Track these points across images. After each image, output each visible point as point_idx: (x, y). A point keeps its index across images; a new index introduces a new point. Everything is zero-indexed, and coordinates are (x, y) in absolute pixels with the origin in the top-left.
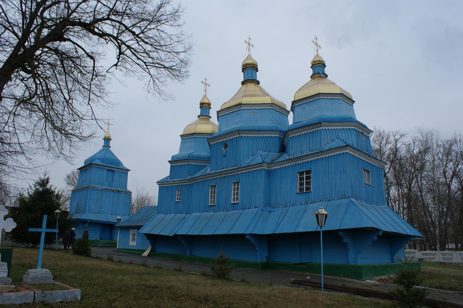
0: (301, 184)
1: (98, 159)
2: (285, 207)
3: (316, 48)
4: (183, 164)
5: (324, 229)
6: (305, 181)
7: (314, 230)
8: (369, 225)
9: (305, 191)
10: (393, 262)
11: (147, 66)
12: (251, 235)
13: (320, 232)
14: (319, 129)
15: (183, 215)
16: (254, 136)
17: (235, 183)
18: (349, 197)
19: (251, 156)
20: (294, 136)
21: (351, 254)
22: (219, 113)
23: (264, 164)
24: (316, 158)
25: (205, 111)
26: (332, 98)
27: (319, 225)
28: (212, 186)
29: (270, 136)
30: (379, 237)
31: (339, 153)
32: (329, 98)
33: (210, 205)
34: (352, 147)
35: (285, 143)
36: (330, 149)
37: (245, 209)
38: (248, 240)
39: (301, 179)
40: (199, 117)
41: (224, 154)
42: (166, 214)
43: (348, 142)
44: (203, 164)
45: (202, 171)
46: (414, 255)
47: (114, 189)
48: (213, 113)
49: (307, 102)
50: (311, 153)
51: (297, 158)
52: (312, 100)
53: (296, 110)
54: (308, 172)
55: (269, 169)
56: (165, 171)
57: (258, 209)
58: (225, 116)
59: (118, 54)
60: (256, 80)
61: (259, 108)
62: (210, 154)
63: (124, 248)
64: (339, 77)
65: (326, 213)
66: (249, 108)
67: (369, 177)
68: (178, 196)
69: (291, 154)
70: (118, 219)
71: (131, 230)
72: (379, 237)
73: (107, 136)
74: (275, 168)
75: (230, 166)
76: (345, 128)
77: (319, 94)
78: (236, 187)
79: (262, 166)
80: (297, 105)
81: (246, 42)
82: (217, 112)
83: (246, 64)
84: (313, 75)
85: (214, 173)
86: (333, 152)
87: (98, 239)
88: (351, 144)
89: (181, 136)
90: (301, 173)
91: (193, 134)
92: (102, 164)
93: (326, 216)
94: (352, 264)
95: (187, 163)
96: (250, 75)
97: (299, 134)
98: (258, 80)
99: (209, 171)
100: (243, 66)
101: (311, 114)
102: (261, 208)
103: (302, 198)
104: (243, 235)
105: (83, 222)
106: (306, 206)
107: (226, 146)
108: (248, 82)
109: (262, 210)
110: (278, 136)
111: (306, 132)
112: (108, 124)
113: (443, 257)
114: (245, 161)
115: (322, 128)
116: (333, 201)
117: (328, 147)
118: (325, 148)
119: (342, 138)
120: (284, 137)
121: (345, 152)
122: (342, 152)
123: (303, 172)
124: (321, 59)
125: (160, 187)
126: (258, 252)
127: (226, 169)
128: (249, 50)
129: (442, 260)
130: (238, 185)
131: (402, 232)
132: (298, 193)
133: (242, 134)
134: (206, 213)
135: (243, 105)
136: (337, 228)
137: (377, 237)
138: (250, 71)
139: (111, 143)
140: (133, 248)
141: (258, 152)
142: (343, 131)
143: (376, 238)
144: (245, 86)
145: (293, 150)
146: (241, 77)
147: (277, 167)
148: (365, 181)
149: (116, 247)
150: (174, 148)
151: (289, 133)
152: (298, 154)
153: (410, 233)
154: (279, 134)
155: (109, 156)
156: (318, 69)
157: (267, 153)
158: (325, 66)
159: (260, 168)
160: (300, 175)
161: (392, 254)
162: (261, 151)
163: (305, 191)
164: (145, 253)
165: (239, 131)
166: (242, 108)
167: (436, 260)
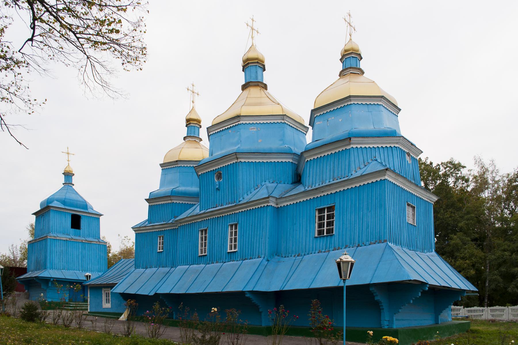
0: (321, 225)
1: (57, 201)
2: (298, 256)
3: (349, 31)
4: (164, 202)
5: (349, 283)
6: (326, 221)
7: (336, 285)
8: (414, 277)
9: (325, 234)
10: (437, 323)
11: (78, 38)
12: (252, 292)
13: (342, 287)
14: (348, 148)
15: (167, 269)
16: (257, 161)
17: (232, 226)
18: (385, 241)
19: (253, 190)
20: (312, 158)
21: (386, 316)
22: (209, 130)
23: (271, 199)
24: (342, 189)
25: (193, 131)
26: (368, 103)
27: (341, 277)
28: (202, 231)
29: (280, 161)
30: (424, 293)
31: (374, 181)
32: (364, 103)
33: (200, 255)
34: (394, 172)
35: (300, 171)
36: (362, 176)
37: (246, 259)
38: (248, 298)
39: (321, 218)
40: (185, 138)
41: (217, 187)
42: (146, 268)
43: (388, 166)
44: (191, 203)
45: (190, 211)
46: (458, 312)
47: (83, 239)
48: (203, 133)
49: (332, 109)
50: (335, 181)
51: (316, 189)
52: (339, 107)
53: (317, 123)
54: (331, 209)
55: (277, 206)
56: (141, 214)
57: (261, 259)
58: (219, 134)
59: (32, 21)
60: (262, 83)
61: (265, 122)
62: (198, 189)
63: (97, 311)
64: (379, 75)
65: (353, 260)
66: (251, 122)
67: (414, 215)
68: (160, 244)
69: (307, 184)
70: (87, 276)
71: (103, 290)
72: (424, 293)
73: (67, 169)
74: (285, 204)
75: (225, 204)
76: (384, 146)
77: (350, 97)
78: (234, 230)
79: (268, 202)
80: (318, 115)
81: (248, 25)
82: (207, 128)
83: (248, 59)
84: (342, 71)
85: (204, 213)
86: (366, 180)
87: (67, 301)
88: (392, 169)
89: (161, 165)
90: (321, 211)
91: (177, 161)
92: (63, 207)
93: (352, 264)
94: (386, 327)
95: (170, 202)
96: (253, 75)
97: (319, 156)
98: (264, 82)
99: (197, 211)
100: (244, 62)
101: (337, 127)
102: (266, 258)
103: (322, 243)
104: (242, 293)
105: (46, 281)
106: (326, 254)
107: (219, 177)
108: (251, 86)
109: (268, 261)
110: (291, 161)
111: (329, 153)
112: (68, 154)
113: (492, 313)
114: (245, 196)
115: (352, 146)
116: (363, 247)
117: (359, 174)
118: (355, 175)
119: (379, 161)
120: (299, 162)
121: (383, 178)
122: (379, 180)
123: (324, 209)
124: (355, 47)
125: (136, 234)
126: (263, 314)
127: (220, 208)
128: (252, 38)
129: (490, 317)
130: (236, 228)
131: (454, 286)
132: (316, 237)
133: (241, 158)
134: (195, 266)
135: (242, 118)
136: (367, 282)
137: (422, 293)
138: (253, 69)
139: (75, 180)
140: (109, 311)
141: (263, 183)
142: (381, 150)
143: (420, 295)
144: (246, 92)
145: (311, 179)
146: (184, 132)
147: (288, 203)
148: (409, 220)
149: (87, 309)
150: (153, 182)
151: (305, 155)
152: (317, 185)
153: (463, 287)
154: (293, 159)
155: (73, 197)
156: (351, 61)
157: (275, 184)
158: (361, 58)
159: (266, 205)
160: (319, 213)
161: (438, 312)
162: (267, 182)
163: (325, 234)
164: (123, 316)
165: (236, 155)
166: (241, 122)
167: (483, 317)
